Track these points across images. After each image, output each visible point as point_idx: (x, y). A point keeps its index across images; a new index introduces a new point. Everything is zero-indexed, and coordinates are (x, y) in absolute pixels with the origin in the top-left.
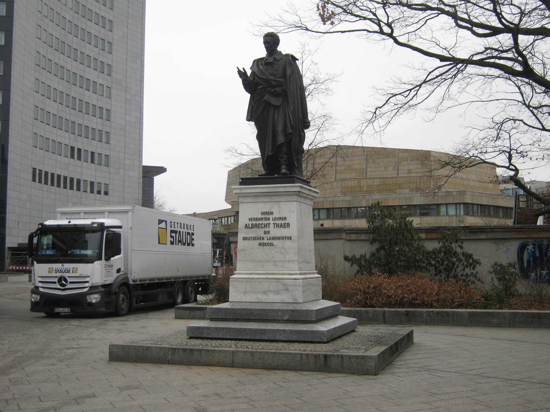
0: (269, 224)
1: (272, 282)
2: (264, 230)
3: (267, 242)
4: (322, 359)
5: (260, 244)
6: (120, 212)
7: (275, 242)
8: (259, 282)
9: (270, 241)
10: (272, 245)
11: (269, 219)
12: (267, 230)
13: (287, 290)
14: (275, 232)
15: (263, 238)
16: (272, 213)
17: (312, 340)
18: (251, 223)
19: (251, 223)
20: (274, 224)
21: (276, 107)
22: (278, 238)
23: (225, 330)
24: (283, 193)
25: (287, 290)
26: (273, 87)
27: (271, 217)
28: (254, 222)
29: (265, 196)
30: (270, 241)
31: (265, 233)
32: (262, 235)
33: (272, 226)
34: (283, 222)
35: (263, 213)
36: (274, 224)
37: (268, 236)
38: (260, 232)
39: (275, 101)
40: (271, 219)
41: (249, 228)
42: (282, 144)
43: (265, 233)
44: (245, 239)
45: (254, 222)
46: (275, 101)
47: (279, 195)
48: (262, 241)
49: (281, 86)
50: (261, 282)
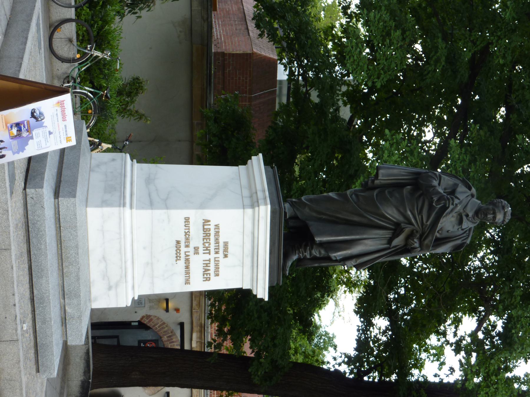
0: (209, 253)
3: (182, 253)
5: (178, 242)
7: (182, 263)
8: (120, 249)
9: (183, 255)
10: (178, 258)
11: (217, 253)
12: (201, 250)
13: (110, 288)
14: (197, 263)
15: (187, 246)
16: (226, 256)
18: (212, 227)
19: (212, 227)
20: (209, 260)
22: (187, 267)
25: (110, 288)
27: (221, 255)
28: (212, 232)
30: (183, 255)
32: (192, 245)
33: (207, 257)
35: (226, 244)
36: (209, 260)
38: (197, 240)
39: (398, 241)
40: (217, 255)
41: (203, 227)
43: (196, 249)
44: (187, 220)
45: (212, 232)
48: (183, 244)
50: (121, 268)
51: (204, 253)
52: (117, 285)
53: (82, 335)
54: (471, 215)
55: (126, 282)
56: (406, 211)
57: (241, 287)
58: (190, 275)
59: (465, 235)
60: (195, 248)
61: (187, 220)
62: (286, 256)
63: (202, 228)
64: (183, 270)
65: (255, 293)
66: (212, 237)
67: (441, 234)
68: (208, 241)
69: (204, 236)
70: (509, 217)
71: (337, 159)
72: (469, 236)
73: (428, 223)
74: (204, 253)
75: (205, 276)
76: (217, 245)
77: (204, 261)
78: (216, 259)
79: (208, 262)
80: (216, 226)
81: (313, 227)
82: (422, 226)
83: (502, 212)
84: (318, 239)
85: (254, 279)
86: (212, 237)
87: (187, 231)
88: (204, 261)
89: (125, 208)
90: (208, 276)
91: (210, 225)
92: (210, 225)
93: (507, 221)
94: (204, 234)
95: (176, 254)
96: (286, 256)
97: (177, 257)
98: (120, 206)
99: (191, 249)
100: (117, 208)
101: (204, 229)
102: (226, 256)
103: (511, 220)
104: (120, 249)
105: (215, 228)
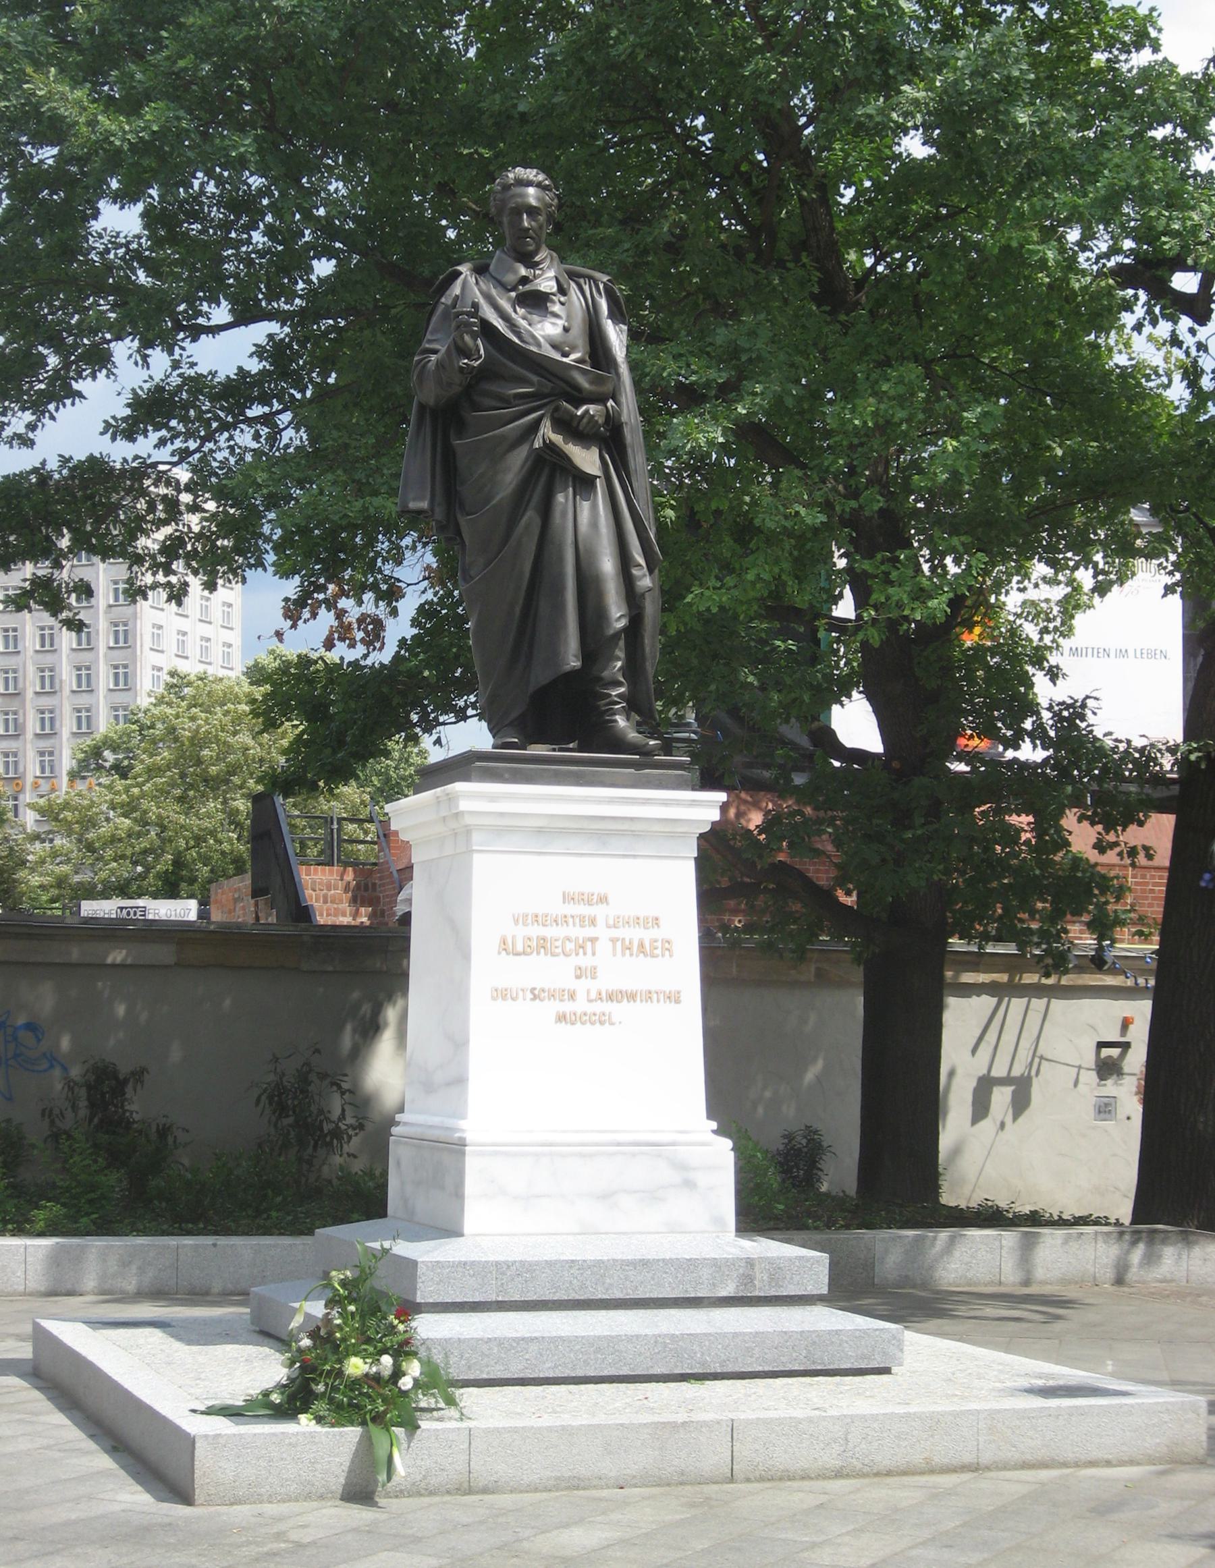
0: (594, 940)
1: (634, 1155)
2: (574, 961)
3: (590, 1008)
4: (22, 1250)
5: (561, 1018)
6: (563, 832)
7: (617, 1010)
8: (582, 1155)
9: (599, 1007)
10: (603, 1020)
11: (593, 922)
12: (585, 961)
13: (689, 1184)
14: (618, 971)
15: (572, 996)
16: (603, 899)
17: (857, 1365)
18: (521, 932)
19: (521, 932)
20: (614, 941)
21: (584, 483)
22: (632, 997)
23: (533, 1347)
24: (657, 827)
25: (689, 1184)
26: (579, 398)
27: (598, 911)
28: (536, 931)
29: (577, 832)
30: (599, 1007)
31: (580, 973)
32: (570, 983)
33: (603, 946)
34: (647, 935)
35: (568, 898)
36: (614, 941)
37: (593, 986)
38: (554, 972)
39: (587, 459)
40: (600, 921)
41: (518, 954)
42: (617, 635)
43: (580, 973)
44: (502, 994)
45: (536, 931)
46: (587, 459)
47: (635, 835)
48: (567, 1007)
49: (600, 399)
50: (634, 1155)
51: (594, 954)
52: (682, 1167)
53: (800, 1258)
54: (523, 271)
55: (673, 1144)
56: (503, 437)
57: (691, 866)
58: (653, 989)
59: (586, 288)
60: (578, 977)
61: (502, 994)
62: (617, 744)
63: (523, 957)
64: (638, 1006)
65: (707, 828)
66: (551, 932)
67: (573, 349)
68: (559, 943)
69: (546, 954)
70: (531, 174)
71: (746, 504)
72: (590, 278)
73: (535, 378)
74: (594, 954)
75: (658, 952)
76: (571, 920)
77: (614, 955)
78: (611, 922)
79: (619, 944)
80: (516, 922)
81: (541, 677)
82: (544, 396)
83: (518, 190)
84: (573, 662)
85: (669, 830)
86: (551, 932)
87: (530, 996)
88: (614, 955)
89: (468, 1141)
90: (659, 944)
91: (514, 937)
92: (514, 937)
93: (541, 177)
94: (538, 953)
95: (593, 1023)
96: (617, 744)
97: (602, 1023)
98: (463, 1153)
99: (581, 986)
100: (467, 1159)
101: (524, 953)
102: (603, 899)
103: (543, 169)
104: (582, 1155)
105: (525, 924)
